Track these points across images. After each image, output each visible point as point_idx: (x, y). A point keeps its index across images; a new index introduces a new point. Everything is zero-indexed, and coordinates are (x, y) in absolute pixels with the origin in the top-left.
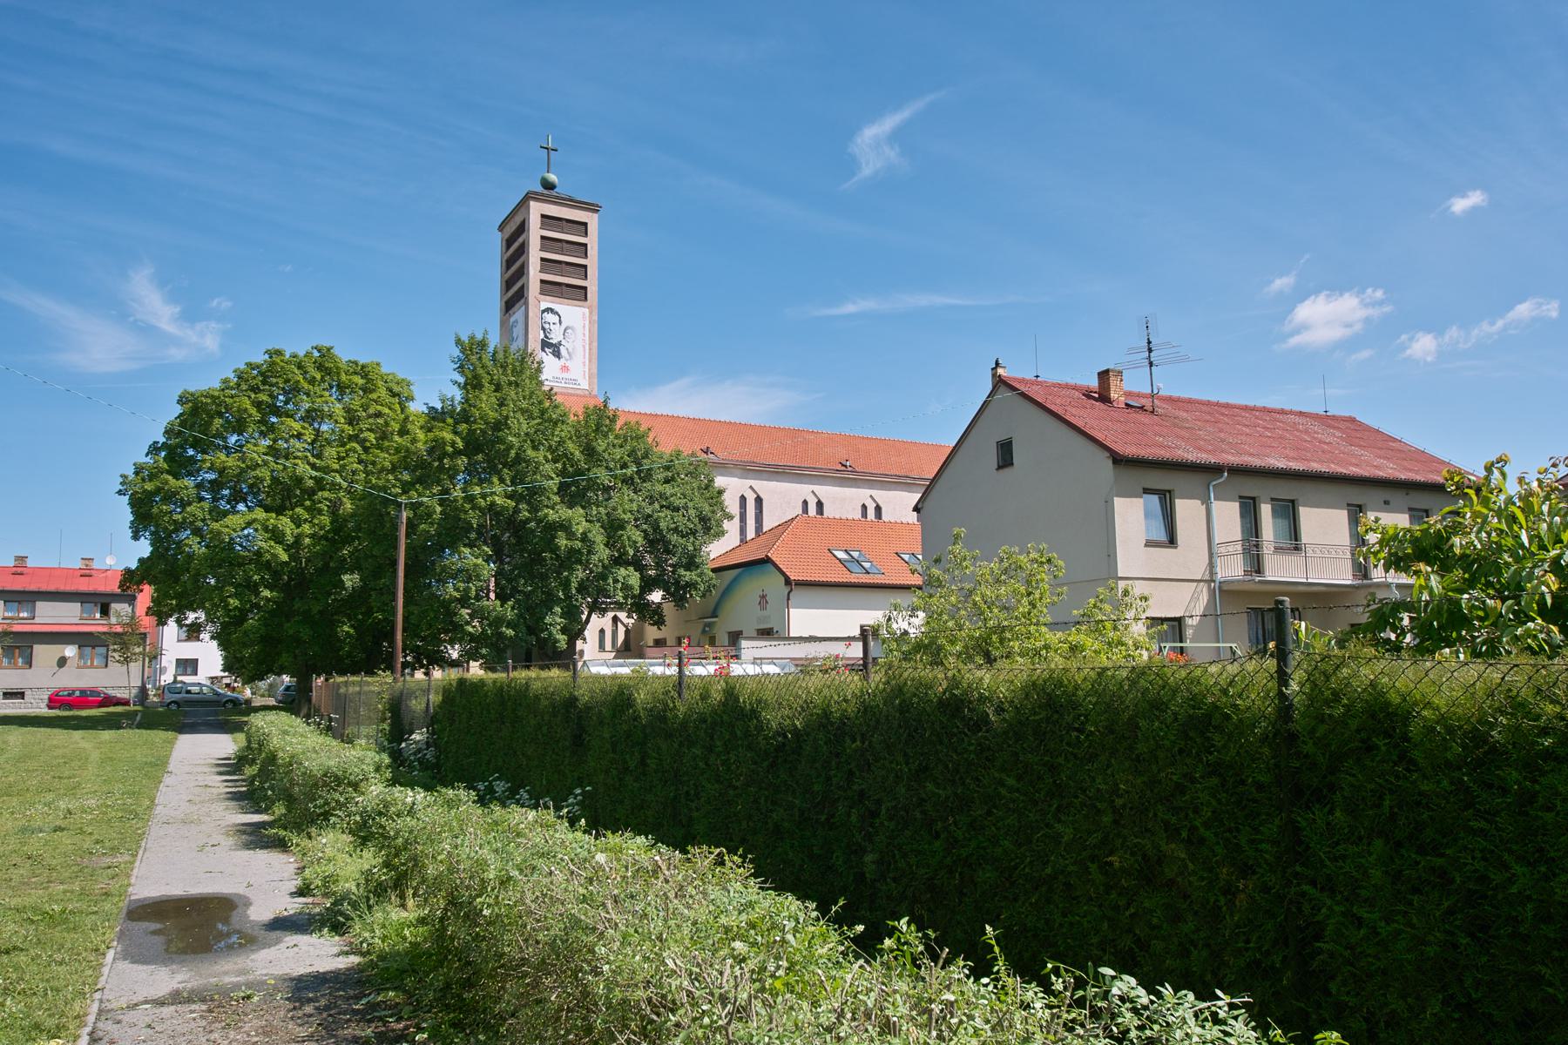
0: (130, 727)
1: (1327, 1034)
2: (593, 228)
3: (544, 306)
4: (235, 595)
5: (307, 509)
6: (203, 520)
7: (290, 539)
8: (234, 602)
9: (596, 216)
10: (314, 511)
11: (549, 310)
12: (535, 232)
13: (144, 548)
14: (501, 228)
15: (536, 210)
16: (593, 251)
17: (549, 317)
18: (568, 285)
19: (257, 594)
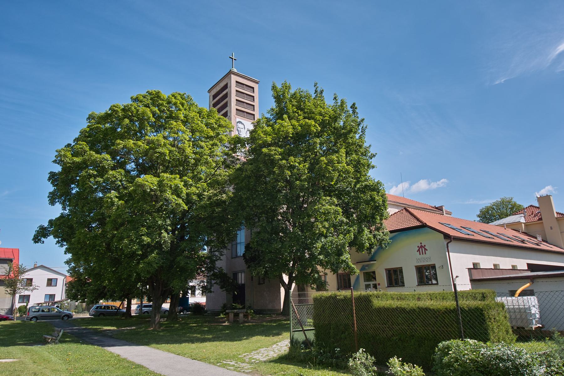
0: (54, 342)
1: (453, 342)
2: (256, 90)
3: (238, 120)
4: (148, 235)
5: (192, 178)
6: (121, 181)
7: (184, 195)
8: (147, 239)
9: (257, 85)
10: (197, 179)
11: (239, 122)
12: (234, 88)
13: (57, 211)
14: (209, 91)
15: (234, 78)
16: (256, 99)
17: (240, 125)
18: (247, 113)
19: (282, 193)
